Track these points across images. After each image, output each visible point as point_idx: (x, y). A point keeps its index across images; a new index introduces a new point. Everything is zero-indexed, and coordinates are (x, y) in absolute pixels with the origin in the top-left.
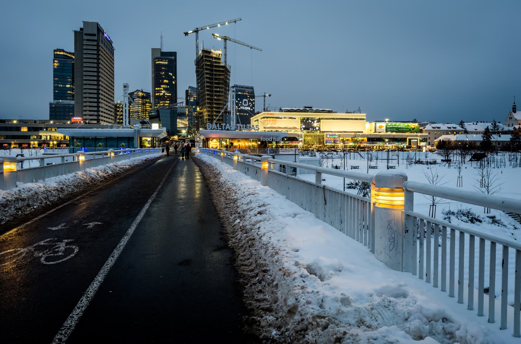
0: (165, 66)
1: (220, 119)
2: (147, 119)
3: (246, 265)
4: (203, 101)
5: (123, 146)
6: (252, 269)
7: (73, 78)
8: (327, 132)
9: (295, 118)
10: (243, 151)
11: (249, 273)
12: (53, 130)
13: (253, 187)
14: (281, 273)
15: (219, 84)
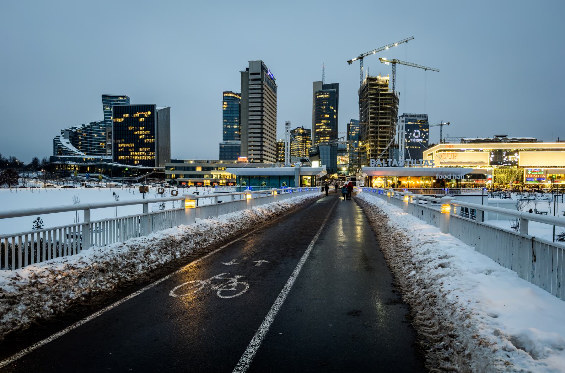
0: (326, 99)
1: (385, 153)
2: (307, 157)
3: (426, 326)
4: (366, 134)
5: (284, 185)
6: (434, 332)
7: (240, 118)
8: (528, 167)
9: (482, 151)
10: (415, 191)
11: (431, 336)
12: (223, 169)
13: (430, 234)
14: (475, 341)
15: (385, 114)
